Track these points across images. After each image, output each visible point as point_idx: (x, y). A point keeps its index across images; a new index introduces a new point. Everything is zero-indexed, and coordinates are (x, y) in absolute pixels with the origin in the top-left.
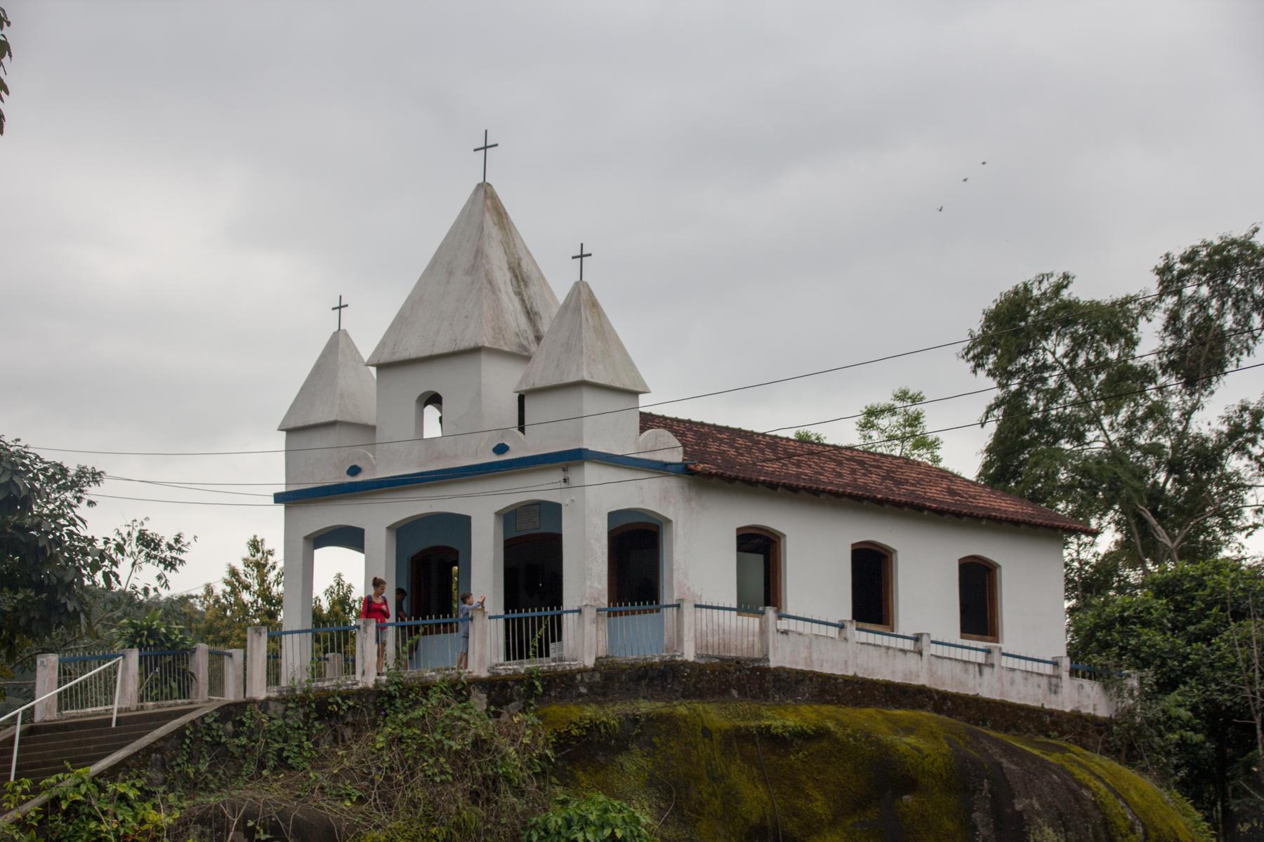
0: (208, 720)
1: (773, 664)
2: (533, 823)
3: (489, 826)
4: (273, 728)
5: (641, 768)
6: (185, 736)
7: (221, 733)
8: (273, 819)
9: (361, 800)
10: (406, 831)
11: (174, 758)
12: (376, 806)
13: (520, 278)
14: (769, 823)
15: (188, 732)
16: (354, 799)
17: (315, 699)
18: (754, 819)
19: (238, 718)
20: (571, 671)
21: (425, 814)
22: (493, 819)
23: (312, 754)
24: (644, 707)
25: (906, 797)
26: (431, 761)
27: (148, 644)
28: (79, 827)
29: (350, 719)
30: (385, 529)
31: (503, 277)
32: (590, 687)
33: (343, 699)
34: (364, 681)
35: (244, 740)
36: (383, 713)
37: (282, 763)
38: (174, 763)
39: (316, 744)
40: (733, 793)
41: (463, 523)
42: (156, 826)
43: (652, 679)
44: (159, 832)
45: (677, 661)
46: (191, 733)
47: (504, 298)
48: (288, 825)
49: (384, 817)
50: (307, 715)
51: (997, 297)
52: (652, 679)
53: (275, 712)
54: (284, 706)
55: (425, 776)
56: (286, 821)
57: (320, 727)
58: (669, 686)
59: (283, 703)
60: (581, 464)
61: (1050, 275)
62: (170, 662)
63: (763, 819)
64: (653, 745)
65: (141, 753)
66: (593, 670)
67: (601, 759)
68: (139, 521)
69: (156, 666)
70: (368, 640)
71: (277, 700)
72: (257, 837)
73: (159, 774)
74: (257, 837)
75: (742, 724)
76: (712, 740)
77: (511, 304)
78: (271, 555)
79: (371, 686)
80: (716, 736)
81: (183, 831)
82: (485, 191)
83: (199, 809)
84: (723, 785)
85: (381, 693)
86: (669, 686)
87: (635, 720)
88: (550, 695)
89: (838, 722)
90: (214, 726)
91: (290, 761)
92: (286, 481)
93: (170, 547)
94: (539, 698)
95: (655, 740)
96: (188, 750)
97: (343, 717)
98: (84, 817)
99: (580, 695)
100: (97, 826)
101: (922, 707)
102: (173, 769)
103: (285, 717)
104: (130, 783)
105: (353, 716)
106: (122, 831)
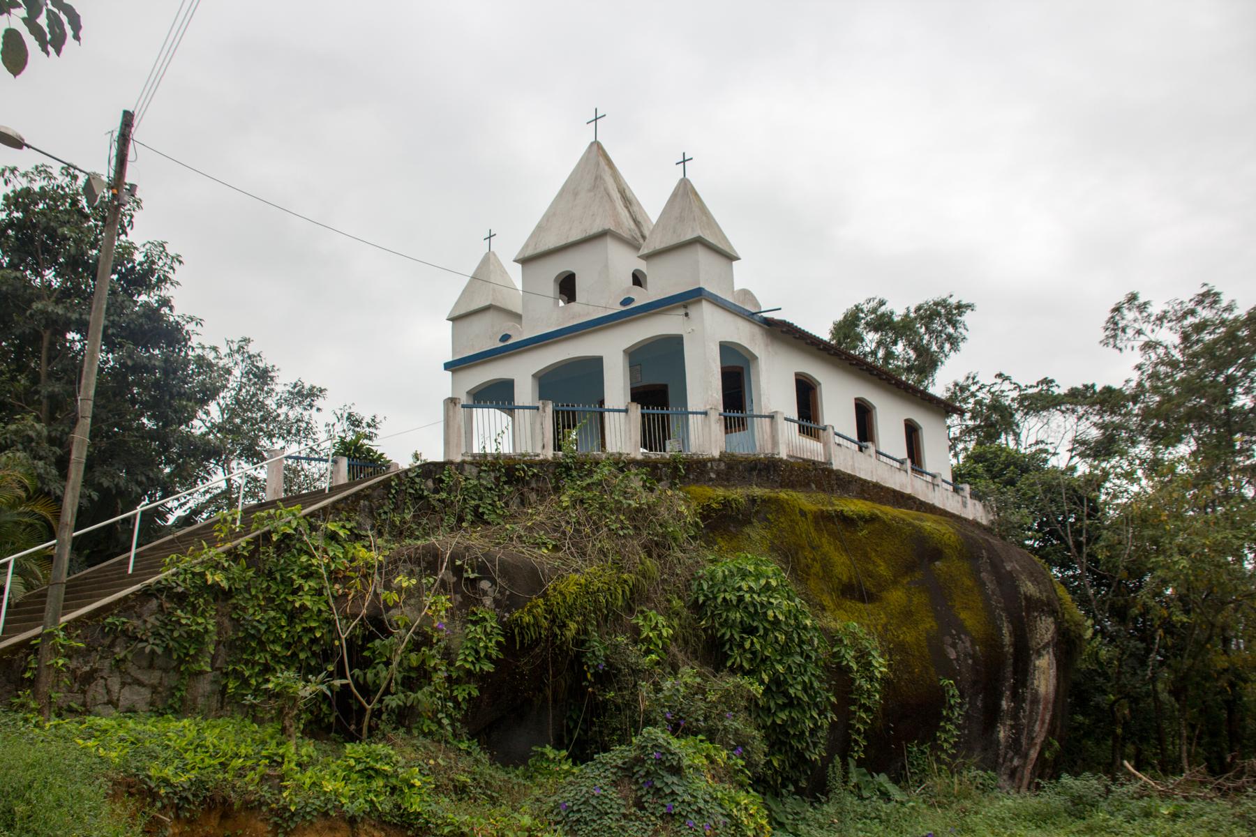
0: (411, 475)
1: (835, 467)
2: (700, 574)
3: (665, 576)
5: (763, 537)
6: (391, 486)
7: (422, 487)
9: (556, 548)
10: (601, 576)
11: (381, 506)
12: (572, 554)
13: (628, 201)
14: (854, 581)
15: (393, 484)
16: (550, 547)
18: (845, 578)
20: (704, 460)
21: (614, 562)
22: (667, 571)
24: (758, 491)
25: (937, 563)
26: (613, 517)
27: (355, 457)
29: (534, 485)
30: (530, 378)
31: (616, 195)
32: (718, 473)
33: (529, 467)
35: (444, 495)
37: (479, 518)
38: (381, 511)
39: (507, 504)
41: (594, 367)
42: (367, 563)
47: (617, 205)
50: (497, 479)
51: (845, 311)
52: (760, 470)
53: (471, 474)
55: (609, 530)
56: (492, 561)
60: (699, 301)
61: (874, 299)
63: (850, 579)
64: (767, 520)
66: (720, 460)
67: (733, 530)
70: (547, 418)
71: (471, 463)
72: (465, 575)
74: (465, 575)
75: (824, 508)
77: (624, 213)
79: (550, 458)
80: (809, 516)
82: (596, 147)
87: (753, 501)
89: (882, 512)
90: (417, 480)
91: (485, 517)
92: (476, 273)
94: (682, 479)
95: (769, 516)
97: (528, 483)
98: (295, 552)
99: (711, 479)
101: (911, 509)
103: (479, 478)
104: (341, 524)
106: (333, 567)
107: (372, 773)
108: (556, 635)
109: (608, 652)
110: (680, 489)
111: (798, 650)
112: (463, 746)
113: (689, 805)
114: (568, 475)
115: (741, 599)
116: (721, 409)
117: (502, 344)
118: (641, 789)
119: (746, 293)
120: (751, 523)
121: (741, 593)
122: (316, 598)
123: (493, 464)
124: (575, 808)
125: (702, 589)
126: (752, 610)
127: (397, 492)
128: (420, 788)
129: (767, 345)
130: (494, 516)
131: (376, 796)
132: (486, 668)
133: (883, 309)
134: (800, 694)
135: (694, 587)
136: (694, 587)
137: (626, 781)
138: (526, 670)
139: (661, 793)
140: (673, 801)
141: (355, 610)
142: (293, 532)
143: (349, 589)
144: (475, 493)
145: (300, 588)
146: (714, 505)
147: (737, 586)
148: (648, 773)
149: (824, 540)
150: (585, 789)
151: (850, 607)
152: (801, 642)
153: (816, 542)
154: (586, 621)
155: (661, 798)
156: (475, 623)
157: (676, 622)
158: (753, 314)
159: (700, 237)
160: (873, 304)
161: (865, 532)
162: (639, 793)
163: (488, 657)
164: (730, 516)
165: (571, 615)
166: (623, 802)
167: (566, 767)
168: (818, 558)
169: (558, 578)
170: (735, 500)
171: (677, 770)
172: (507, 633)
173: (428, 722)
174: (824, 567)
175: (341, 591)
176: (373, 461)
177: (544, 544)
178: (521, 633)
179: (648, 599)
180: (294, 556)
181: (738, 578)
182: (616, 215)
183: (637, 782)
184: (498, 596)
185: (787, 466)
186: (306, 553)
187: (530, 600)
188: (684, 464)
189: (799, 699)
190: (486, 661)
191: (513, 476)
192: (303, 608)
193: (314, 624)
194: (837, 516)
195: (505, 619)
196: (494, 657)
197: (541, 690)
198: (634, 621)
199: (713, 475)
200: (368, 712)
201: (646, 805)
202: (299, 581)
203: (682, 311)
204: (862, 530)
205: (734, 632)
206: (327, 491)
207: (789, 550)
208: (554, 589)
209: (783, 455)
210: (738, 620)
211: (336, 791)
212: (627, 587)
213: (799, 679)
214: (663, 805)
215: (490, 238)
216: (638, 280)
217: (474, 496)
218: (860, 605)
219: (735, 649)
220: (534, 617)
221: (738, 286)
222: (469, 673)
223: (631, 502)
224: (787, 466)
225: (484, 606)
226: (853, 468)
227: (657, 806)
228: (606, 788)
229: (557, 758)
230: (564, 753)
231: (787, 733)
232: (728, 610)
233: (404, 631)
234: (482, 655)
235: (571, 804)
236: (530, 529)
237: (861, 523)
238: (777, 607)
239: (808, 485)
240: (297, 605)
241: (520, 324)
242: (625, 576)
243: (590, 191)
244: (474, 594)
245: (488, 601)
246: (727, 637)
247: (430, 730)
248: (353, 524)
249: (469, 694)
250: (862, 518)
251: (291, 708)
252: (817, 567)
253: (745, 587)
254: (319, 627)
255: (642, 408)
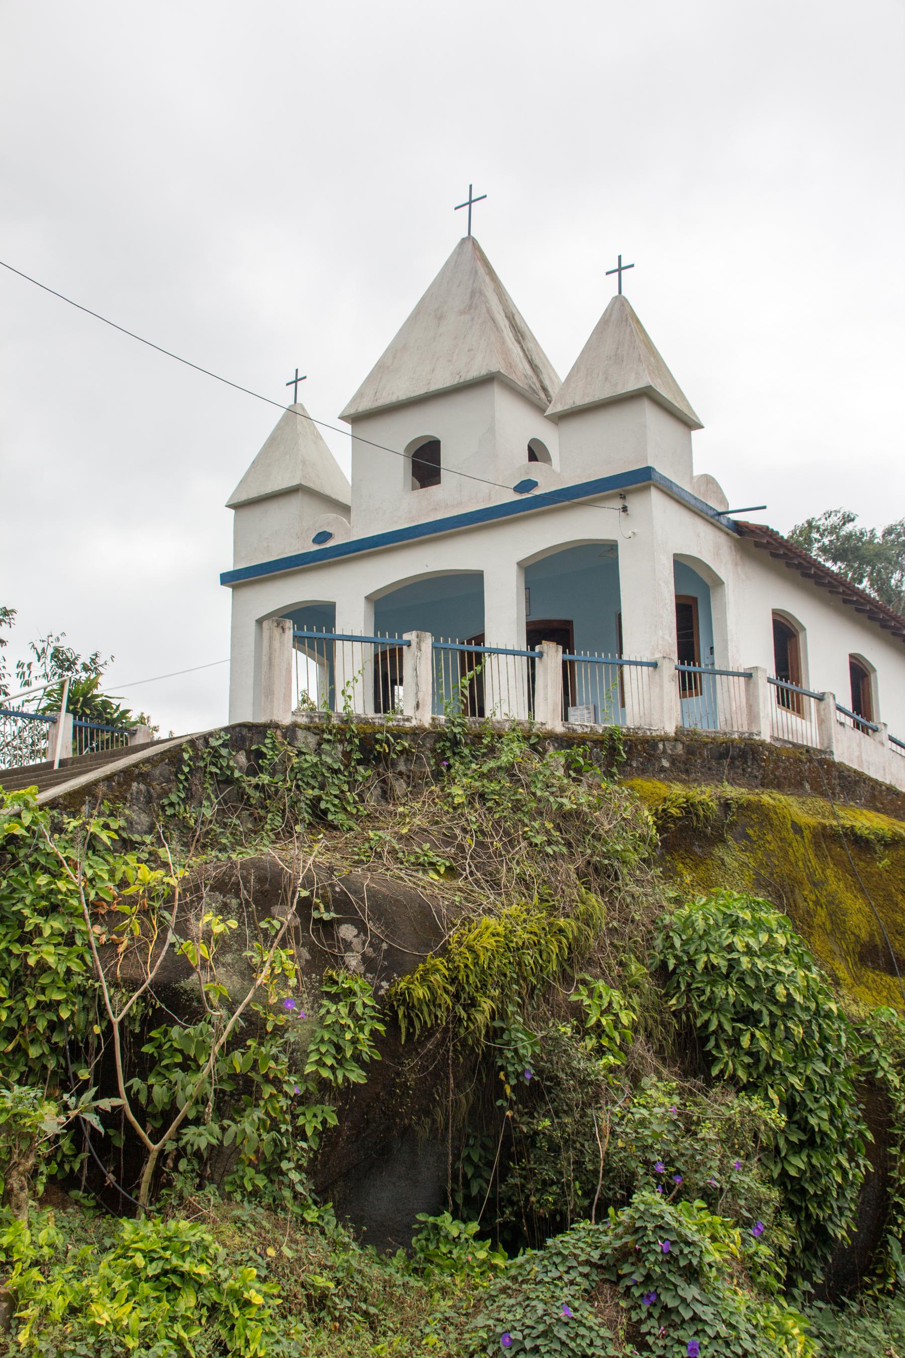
0: (214, 743)
1: (837, 758)
2: (667, 922)
3: (615, 923)
4: (306, 765)
5: (743, 864)
6: (181, 761)
7: (232, 763)
8: (337, 889)
10: (525, 921)
11: (165, 793)
12: (477, 882)
13: (520, 333)
15: (186, 756)
16: (442, 870)
17: (358, 734)
19: (254, 747)
23: (358, 810)
24: (731, 792)
27: (84, 713)
28: (19, 882)
29: (402, 767)
30: (363, 600)
31: (503, 323)
32: (673, 760)
34: (419, 717)
35: (265, 778)
36: (445, 763)
37: (320, 818)
38: (165, 801)
40: (837, 902)
43: (733, 758)
44: (152, 899)
45: (754, 740)
46: (190, 759)
48: (362, 899)
49: (492, 897)
50: (347, 755)
53: (307, 746)
54: (318, 737)
55: (531, 844)
57: (366, 774)
58: (749, 770)
59: (315, 734)
60: (647, 488)
62: (108, 740)
63: (872, 936)
64: (747, 837)
65: (116, 778)
67: (698, 850)
68: (55, 636)
69: (86, 746)
70: (423, 661)
71: (308, 728)
73: (143, 816)
74: (315, 915)
75: (827, 822)
76: (803, 837)
77: (516, 349)
78: (157, 731)
79: (427, 725)
80: (806, 833)
81: (192, 901)
83: (216, 868)
84: (825, 893)
85: (441, 736)
86: (749, 770)
87: (726, 805)
88: (631, 766)
90: (224, 752)
91: (330, 817)
93: (86, 668)
94: (622, 766)
95: (750, 832)
96: (186, 784)
97: (394, 764)
98: (27, 868)
99: (662, 770)
100: (48, 884)
102: (164, 811)
103: (318, 752)
104: (102, 820)
105: (406, 764)
107: (175, 1280)
108: (460, 1020)
109: (537, 1050)
110: (619, 783)
111: (820, 1052)
112: (311, 1215)
113: (727, 1344)
114: (454, 754)
115: (733, 964)
116: (676, 661)
117: (316, 547)
118: (635, 1307)
119: (709, 481)
120: (724, 841)
121: (734, 955)
122: (63, 950)
123: (341, 731)
124: (528, 1344)
125: (672, 946)
126: (752, 983)
127: (190, 772)
128: (261, 1308)
129: (736, 565)
130: (341, 816)
131: (186, 1328)
132: (353, 1077)
133: (849, 527)
134: (826, 1126)
135: (659, 942)
136: (659, 942)
137: (607, 1290)
138: (411, 1079)
139: (673, 1317)
140: (696, 1333)
141: (131, 972)
142: (24, 832)
143: (120, 934)
144: (314, 777)
145: (38, 931)
146: (674, 811)
147: (726, 943)
148: (648, 1278)
149: (828, 872)
150: (540, 1307)
151: (874, 981)
152: (825, 1039)
153: (818, 876)
154: (505, 997)
155: (675, 1326)
156: (335, 998)
157: (636, 1001)
158: (720, 514)
159: (650, 387)
160: (834, 520)
161: (886, 862)
162: (635, 1317)
163: (357, 1058)
164: (695, 830)
165: (484, 985)
166: (608, 1334)
167: (482, 1255)
168: (823, 900)
169: (463, 924)
170: (701, 803)
171: (693, 1274)
172: (385, 1015)
173: (250, 1172)
174: (831, 915)
175: (104, 938)
176: (111, 722)
177: (432, 864)
178: (408, 1016)
179: (590, 962)
180: (24, 874)
181: (726, 931)
182: (505, 353)
183: (627, 1293)
184: (369, 951)
185: (771, 752)
186: (46, 870)
187: (424, 960)
188: (625, 744)
189: (823, 1134)
190: (353, 1066)
191: (371, 752)
192: (43, 967)
193: (58, 996)
194: (846, 835)
195: (382, 992)
196: (366, 1057)
197: (428, 1113)
198: (574, 998)
199: (666, 764)
200: (153, 1156)
201: (650, 1340)
202: (33, 920)
203: (618, 504)
204: (881, 859)
205: (723, 1019)
206: (56, 767)
207: (782, 886)
208: (460, 943)
209: (766, 736)
210: (732, 1000)
211: (116, 1323)
212: (564, 941)
213: (823, 1100)
214: (680, 1342)
215: (296, 382)
216: (536, 452)
217: (312, 782)
218: (888, 979)
219: (724, 1047)
220: (429, 988)
221: (697, 471)
222: (324, 1085)
223: (565, 801)
224: (771, 752)
225: (347, 968)
226: (861, 762)
227: (668, 1342)
228: (576, 1304)
229: (463, 1236)
230: (474, 1227)
231: (803, 1192)
232: (713, 983)
233: (223, 1012)
234: (348, 1054)
235: (519, 1336)
236: (406, 839)
237: (879, 848)
238: (789, 981)
239: (799, 785)
240: (32, 961)
241: (349, 519)
242: (562, 922)
243: (462, 313)
244: (331, 946)
245: (353, 960)
246: (713, 1027)
247: (254, 1185)
248: (122, 822)
249: (324, 1122)
250: (881, 839)
251: (24, 1155)
252: (821, 916)
253: (740, 946)
254: (67, 1001)
255: (564, 652)
